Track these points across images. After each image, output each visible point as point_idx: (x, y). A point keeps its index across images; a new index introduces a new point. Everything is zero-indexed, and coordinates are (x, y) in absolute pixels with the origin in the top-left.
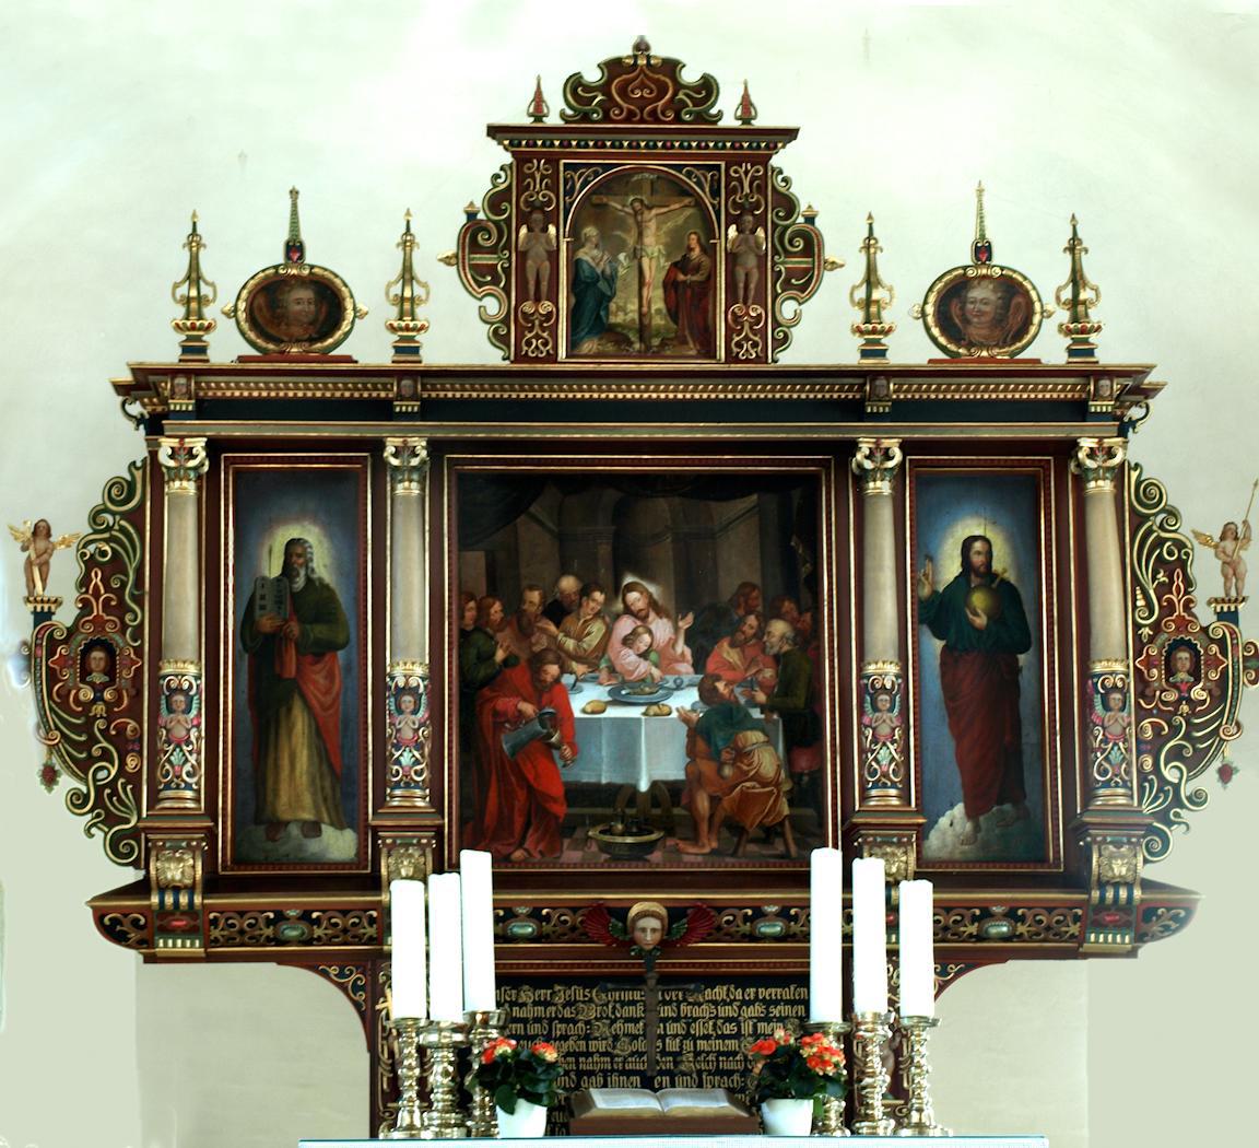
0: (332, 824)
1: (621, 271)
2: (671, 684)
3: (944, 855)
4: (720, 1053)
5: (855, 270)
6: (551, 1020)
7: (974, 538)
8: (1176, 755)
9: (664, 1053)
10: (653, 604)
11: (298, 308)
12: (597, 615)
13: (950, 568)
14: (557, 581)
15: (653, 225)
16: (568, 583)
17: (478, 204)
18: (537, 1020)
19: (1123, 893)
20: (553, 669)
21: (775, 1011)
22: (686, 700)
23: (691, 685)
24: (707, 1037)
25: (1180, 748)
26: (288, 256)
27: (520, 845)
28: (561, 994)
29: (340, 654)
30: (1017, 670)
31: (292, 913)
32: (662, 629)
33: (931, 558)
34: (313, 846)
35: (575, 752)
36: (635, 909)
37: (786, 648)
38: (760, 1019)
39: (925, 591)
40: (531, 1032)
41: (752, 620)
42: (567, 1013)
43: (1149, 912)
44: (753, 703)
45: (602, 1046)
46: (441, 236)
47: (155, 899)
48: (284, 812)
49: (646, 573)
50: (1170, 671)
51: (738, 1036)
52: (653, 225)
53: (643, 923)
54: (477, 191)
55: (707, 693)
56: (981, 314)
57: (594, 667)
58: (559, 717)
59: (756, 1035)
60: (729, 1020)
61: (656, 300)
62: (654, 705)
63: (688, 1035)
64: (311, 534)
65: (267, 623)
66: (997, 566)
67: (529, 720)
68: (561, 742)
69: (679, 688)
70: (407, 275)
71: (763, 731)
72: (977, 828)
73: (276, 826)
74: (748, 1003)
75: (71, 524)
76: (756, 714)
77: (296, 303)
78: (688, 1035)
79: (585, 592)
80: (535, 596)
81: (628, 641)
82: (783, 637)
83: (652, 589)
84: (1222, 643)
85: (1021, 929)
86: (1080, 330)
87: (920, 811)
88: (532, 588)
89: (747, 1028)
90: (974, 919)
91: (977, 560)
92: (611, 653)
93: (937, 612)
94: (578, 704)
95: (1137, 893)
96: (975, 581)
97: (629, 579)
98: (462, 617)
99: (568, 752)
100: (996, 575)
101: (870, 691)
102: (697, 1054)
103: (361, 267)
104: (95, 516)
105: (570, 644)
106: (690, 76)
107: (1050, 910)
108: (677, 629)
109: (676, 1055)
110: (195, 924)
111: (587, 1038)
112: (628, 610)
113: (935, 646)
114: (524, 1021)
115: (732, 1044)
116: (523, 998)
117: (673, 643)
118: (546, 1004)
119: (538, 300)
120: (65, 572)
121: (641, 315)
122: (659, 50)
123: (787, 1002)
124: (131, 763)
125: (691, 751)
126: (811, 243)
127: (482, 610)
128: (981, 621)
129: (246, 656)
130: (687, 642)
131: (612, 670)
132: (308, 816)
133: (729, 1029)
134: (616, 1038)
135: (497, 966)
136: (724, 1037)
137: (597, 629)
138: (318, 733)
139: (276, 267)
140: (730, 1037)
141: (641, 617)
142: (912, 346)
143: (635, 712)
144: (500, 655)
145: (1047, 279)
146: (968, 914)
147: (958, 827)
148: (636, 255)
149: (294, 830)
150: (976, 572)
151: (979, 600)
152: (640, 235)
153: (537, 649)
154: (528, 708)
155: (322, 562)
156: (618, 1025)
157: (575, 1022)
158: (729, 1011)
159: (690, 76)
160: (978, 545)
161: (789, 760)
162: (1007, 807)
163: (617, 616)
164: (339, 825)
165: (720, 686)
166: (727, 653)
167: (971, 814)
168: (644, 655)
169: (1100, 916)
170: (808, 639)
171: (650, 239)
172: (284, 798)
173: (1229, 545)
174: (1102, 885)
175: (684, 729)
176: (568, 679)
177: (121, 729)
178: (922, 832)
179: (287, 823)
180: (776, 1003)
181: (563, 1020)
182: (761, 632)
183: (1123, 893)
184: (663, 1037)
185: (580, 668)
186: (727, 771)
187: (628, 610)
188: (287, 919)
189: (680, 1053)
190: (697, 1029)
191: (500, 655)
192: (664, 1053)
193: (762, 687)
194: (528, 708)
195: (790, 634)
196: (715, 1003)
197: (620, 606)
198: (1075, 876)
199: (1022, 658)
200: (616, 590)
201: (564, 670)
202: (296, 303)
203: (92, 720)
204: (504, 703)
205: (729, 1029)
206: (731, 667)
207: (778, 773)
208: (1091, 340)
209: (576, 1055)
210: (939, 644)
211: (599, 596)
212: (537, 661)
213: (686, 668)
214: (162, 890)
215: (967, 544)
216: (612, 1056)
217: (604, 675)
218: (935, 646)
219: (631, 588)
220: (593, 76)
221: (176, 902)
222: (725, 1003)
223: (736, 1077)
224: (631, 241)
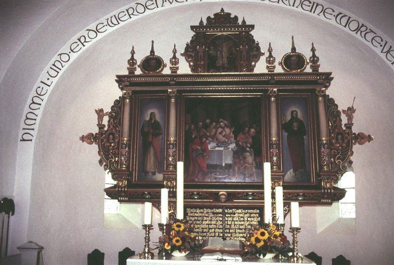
0: (158, 172)
1: (218, 55)
2: (229, 142)
3: (288, 181)
4: (239, 225)
5: (267, 54)
6: (203, 217)
7: (293, 111)
8: (339, 158)
9: (227, 224)
10: (226, 125)
11: (153, 64)
12: (214, 128)
13: (289, 118)
14: (205, 120)
15: (225, 46)
16: (208, 121)
17: (189, 43)
18: (200, 216)
19: (329, 191)
20: (204, 139)
21: (252, 215)
22: (232, 146)
23: (234, 143)
24: (237, 221)
25: (339, 157)
26: (151, 54)
27: (197, 177)
28: (206, 211)
29: (161, 136)
30: (303, 139)
31: (195, 193)
32: (228, 130)
33: (284, 115)
34: (154, 177)
35: (208, 157)
36: (221, 193)
37: (254, 135)
38: (249, 217)
39: (283, 122)
40: (199, 219)
41: (247, 129)
42: (207, 215)
43: (335, 195)
44: (247, 147)
45: (214, 222)
46: (181, 49)
47: (117, 189)
48: (148, 171)
49: (225, 119)
50: (337, 139)
51: (244, 221)
52: (225, 46)
53: (221, 197)
54: (189, 40)
55: (237, 145)
56: (294, 63)
57: (213, 139)
58: (205, 150)
59: (248, 221)
60: (242, 217)
61: (225, 60)
62: (226, 147)
63: (233, 220)
64: (155, 111)
65: (146, 130)
66: (299, 117)
67: (199, 150)
68: (206, 155)
69: (231, 143)
70: (174, 57)
71: (249, 153)
72: (296, 175)
73: (147, 173)
74: (246, 213)
75: (107, 109)
76: (248, 149)
77: (153, 63)
78: (233, 220)
79: (211, 123)
80: (201, 124)
81: (221, 133)
82: (253, 132)
83: (226, 122)
84: (348, 133)
85: (306, 198)
86: (315, 67)
87: (283, 172)
88: (200, 122)
89: (246, 219)
90: (295, 196)
91: (294, 116)
92: (217, 136)
93: (284, 127)
94: (210, 147)
95: (332, 191)
96: (294, 120)
97: (221, 120)
98: (185, 128)
99: (207, 157)
100: (298, 119)
101: (271, 145)
102: (235, 225)
103: (165, 56)
104: (112, 108)
105: (208, 134)
106: (232, 16)
107: (312, 194)
108: (231, 130)
109: (230, 225)
110: (126, 194)
111: (211, 221)
112: (220, 127)
113: (286, 134)
114: (197, 217)
115: (242, 223)
116: (197, 211)
117: (230, 134)
118: (202, 213)
119: (201, 61)
120: (106, 120)
121: (222, 64)
122: (226, 11)
123: (255, 213)
124: (117, 159)
125: (234, 157)
126: (258, 48)
127: (190, 127)
128: (296, 129)
129: (142, 137)
130: (233, 133)
131: (217, 139)
132: (153, 171)
133: (242, 219)
134: (217, 221)
135: (184, 202)
136: (241, 221)
137: (214, 130)
138: (155, 154)
139: (148, 56)
140: (242, 221)
141: (223, 128)
142: (279, 69)
143: (222, 149)
144: (193, 136)
145: (308, 55)
146: (243, 195)
147: (291, 174)
148: (221, 52)
149: (150, 174)
150: (294, 118)
151: (295, 124)
152: (222, 48)
153: (201, 135)
154: (199, 148)
155: (158, 117)
156: (218, 218)
157: (208, 217)
158: (242, 215)
159: (232, 16)
160: (295, 112)
161: (255, 160)
162: (302, 170)
163: (218, 128)
164: (159, 172)
165: (240, 143)
166: (241, 136)
167: (294, 171)
168: (224, 136)
169: (323, 196)
170: (259, 132)
171: (224, 49)
172: (148, 168)
173: (349, 112)
174: (324, 189)
175: (232, 153)
176: (208, 141)
177: (115, 152)
178: (283, 176)
179: (149, 172)
180: (252, 213)
181: (206, 217)
182: (249, 131)
183: (329, 191)
184: (227, 221)
185: (210, 139)
186: (242, 162)
187: (220, 127)
188: (194, 194)
189: (231, 225)
190: (235, 219)
191: (193, 136)
192: (227, 224)
193: (249, 143)
194: (199, 148)
195: (255, 131)
196: (239, 213)
197: (219, 126)
198: (318, 187)
199: (305, 137)
200: (218, 122)
201: (207, 139)
202: (153, 63)
203: (109, 150)
204: (194, 147)
205: (242, 219)
206: (243, 139)
207: (252, 162)
208: (267, 71)
209: (209, 224)
210: (287, 134)
211: (214, 124)
212: (201, 138)
213: (233, 139)
214: (324, 189)
215: (292, 112)
216: (216, 225)
217: (215, 140)
218: (286, 134)
219: (221, 122)
220: (212, 17)
221: (121, 190)
222: (241, 213)
223: (243, 230)
224: (220, 49)
